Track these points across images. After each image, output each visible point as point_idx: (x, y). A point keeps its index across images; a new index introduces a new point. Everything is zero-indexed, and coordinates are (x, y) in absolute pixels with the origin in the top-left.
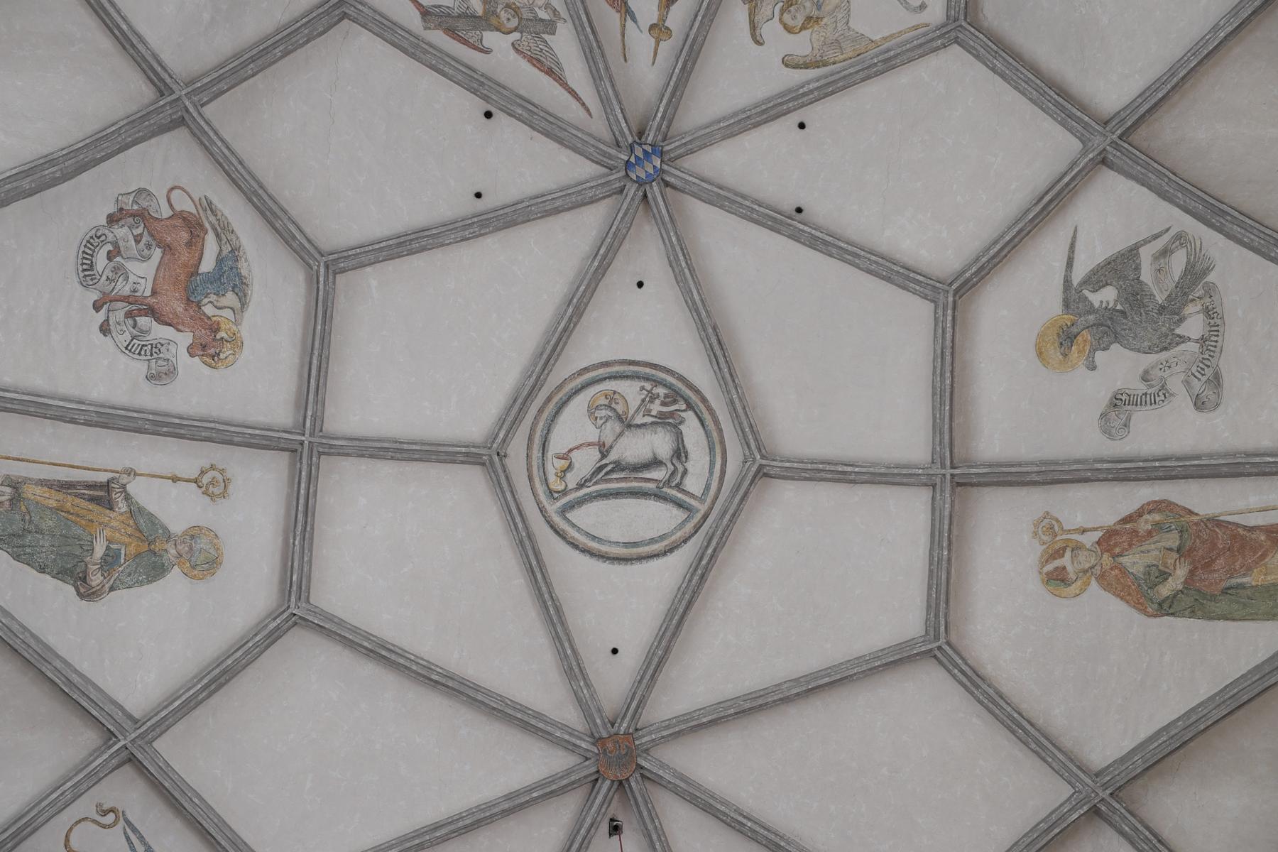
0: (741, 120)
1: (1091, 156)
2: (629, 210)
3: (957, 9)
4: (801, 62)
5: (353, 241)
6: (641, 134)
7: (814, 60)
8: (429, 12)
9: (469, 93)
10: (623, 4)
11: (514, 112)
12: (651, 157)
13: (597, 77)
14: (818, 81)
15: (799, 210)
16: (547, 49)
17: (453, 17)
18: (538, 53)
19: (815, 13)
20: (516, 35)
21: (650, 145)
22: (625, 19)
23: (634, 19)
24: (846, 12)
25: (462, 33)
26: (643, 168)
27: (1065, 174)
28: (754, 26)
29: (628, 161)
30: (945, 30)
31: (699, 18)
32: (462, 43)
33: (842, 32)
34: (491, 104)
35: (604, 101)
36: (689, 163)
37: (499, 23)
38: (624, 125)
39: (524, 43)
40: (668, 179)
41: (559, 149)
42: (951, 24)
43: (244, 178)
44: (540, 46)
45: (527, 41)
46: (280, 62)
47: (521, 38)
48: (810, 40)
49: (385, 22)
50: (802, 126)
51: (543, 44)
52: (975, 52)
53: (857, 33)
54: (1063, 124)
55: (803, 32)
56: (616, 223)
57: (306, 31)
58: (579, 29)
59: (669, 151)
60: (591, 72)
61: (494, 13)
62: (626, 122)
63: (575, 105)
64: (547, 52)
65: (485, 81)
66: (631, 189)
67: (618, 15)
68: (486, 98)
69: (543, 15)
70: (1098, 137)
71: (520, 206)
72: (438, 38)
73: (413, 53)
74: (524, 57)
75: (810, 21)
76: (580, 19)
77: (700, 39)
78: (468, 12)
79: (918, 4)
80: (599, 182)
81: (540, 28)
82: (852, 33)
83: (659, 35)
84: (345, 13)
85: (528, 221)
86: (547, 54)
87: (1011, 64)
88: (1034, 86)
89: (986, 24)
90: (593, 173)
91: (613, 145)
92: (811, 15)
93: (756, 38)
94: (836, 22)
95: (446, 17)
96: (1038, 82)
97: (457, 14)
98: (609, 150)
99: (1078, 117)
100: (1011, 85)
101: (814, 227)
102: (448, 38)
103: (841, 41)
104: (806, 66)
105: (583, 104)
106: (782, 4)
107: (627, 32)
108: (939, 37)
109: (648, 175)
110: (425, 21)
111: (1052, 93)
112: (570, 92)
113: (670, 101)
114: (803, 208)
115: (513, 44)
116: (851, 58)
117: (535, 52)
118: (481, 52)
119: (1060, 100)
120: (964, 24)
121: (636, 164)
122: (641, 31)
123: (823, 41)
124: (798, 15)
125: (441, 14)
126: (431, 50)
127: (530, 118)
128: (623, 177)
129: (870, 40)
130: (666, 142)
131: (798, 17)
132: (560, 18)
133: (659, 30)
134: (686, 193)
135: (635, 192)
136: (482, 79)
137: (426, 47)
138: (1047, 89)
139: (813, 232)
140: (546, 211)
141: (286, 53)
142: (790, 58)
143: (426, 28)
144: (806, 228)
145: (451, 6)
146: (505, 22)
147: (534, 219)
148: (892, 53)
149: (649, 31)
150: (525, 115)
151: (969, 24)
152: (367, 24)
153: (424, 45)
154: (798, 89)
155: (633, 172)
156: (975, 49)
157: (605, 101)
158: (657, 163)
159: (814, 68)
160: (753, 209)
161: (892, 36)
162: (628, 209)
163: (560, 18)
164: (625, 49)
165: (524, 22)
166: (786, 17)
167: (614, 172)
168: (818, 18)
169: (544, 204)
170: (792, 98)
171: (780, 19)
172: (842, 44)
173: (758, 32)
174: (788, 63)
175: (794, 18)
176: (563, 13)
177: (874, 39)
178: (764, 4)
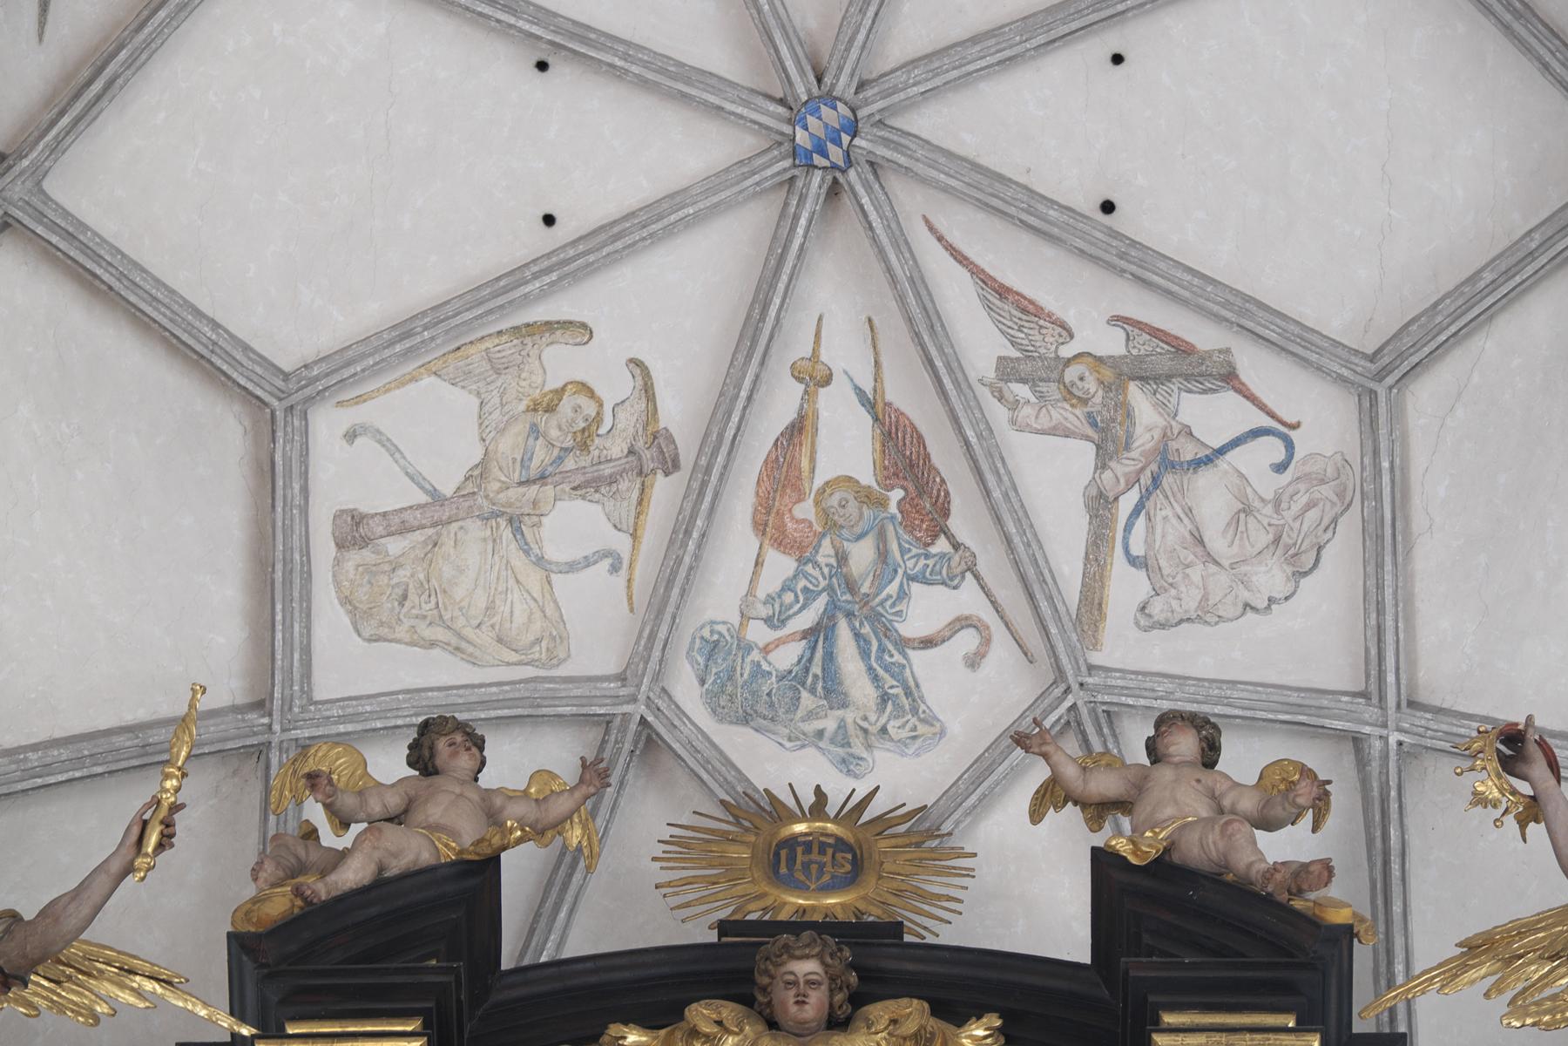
0: (658, 221)
1: (25, 163)
2: (845, 50)
3: (289, 429)
4: (559, 333)
5: (1425, 702)
6: (834, 191)
7: (537, 337)
8: (1222, 381)
9: (1145, 243)
10: (881, 417)
11: (1062, 212)
12: (813, 146)
13: (918, 282)
14: (526, 296)
15: (542, 66)
16: (1010, 331)
17: (1180, 375)
18: (1026, 324)
19: (541, 419)
20: (1067, 351)
21: (816, 167)
22: (875, 391)
23: (859, 392)
24: (486, 423)
25: (1163, 349)
26: (826, 125)
27: (68, 131)
28: (646, 391)
29: (854, 136)
30: (308, 391)
31: (744, 394)
32: (1162, 331)
33: (491, 388)
34: (1103, 225)
35: (902, 243)
36: (748, 143)
37: (1097, 371)
38: (865, 200)
39: (1052, 340)
40: (781, 110)
41: (978, 156)
42: (298, 403)
43: (1537, 38)
44: (1023, 336)
45: (1046, 342)
46: (1484, 263)
47: (1057, 348)
48: (545, 372)
49: (1300, 351)
50: (549, 220)
51: (1019, 341)
52: (251, 355)
53: (463, 387)
54: (84, 227)
55: (558, 385)
56: (867, 22)
57: (1439, 318)
58: (956, 367)
59: (783, 158)
60: (930, 294)
61: (1107, 387)
62: (861, 207)
63: (955, 238)
64: (1009, 327)
65: (1116, 261)
66: (843, 85)
67: (889, 397)
68: (1114, 234)
69: (1022, 391)
70: (16, 197)
71: (1041, 39)
72: (1204, 336)
73: (1248, 301)
74: (1050, 315)
75: (548, 404)
76: (956, 383)
77: (741, 358)
78: (1155, 387)
79: (359, 441)
80: (902, 95)
81: (1026, 368)
82: (474, 387)
83: (814, 368)
84: (1371, 361)
85: (1025, 18)
86: (1009, 324)
87: (185, 331)
88: (140, 292)
89: (237, 407)
90: (916, 117)
91: (882, 167)
92: (547, 415)
93: (642, 371)
94: (502, 405)
95: (1193, 375)
96: (132, 298)
97: (1174, 380)
98: (888, 154)
99: (54, 232)
100: (181, 297)
101: (512, 32)
102: (1188, 339)
103: (491, 372)
104: (549, 326)
105: (940, 239)
106: (600, 432)
107: (871, 368)
108: (317, 379)
109: (816, 112)
110: (1230, 364)
111: (106, 277)
112: (966, 258)
113: (786, 248)
114: (536, 70)
115: (1071, 336)
116: (471, 343)
117: (1032, 325)
118: (1127, 318)
119: (90, 265)
120: (275, 403)
121: (838, 131)
122: (846, 373)
123: (521, 370)
124: (570, 414)
125: (1201, 379)
126: (1216, 308)
127: (1032, 202)
128: (860, 107)
129: (439, 376)
130: (788, 175)
131: (569, 410)
132: (991, 386)
133: (814, 377)
134: (747, 89)
135: (838, 80)
136: (1123, 264)
137: (1224, 313)
138: (116, 285)
139: (512, 20)
140: (995, 36)
141: (1472, 279)
142: (578, 340)
143: (1228, 351)
144: (527, 27)
145: (1184, 394)
146: (1087, 374)
147: (1017, 21)
148: (398, 348)
149: (831, 375)
150: (1041, 208)
151: (266, 404)
152: (1331, 345)
153: (1229, 315)
154: (560, 279)
155: (844, 117)
156: (250, 359)
157: (901, 242)
158: (801, 137)
159: (536, 323)
160: (625, 60)
161: (402, 383)
162: (848, 50)
163: (991, 386)
164: (873, 339)
165: (1055, 375)
166: (590, 409)
167: (877, 117)
168: (535, 410)
169: (998, 47)
170: (569, 264)
171: (601, 406)
172: (489, 367)
173: (639, 382)
174: (581, 331)
175: (577, 409)
176: (985, 395)
177: (433, 379)
178: (631, 430)
